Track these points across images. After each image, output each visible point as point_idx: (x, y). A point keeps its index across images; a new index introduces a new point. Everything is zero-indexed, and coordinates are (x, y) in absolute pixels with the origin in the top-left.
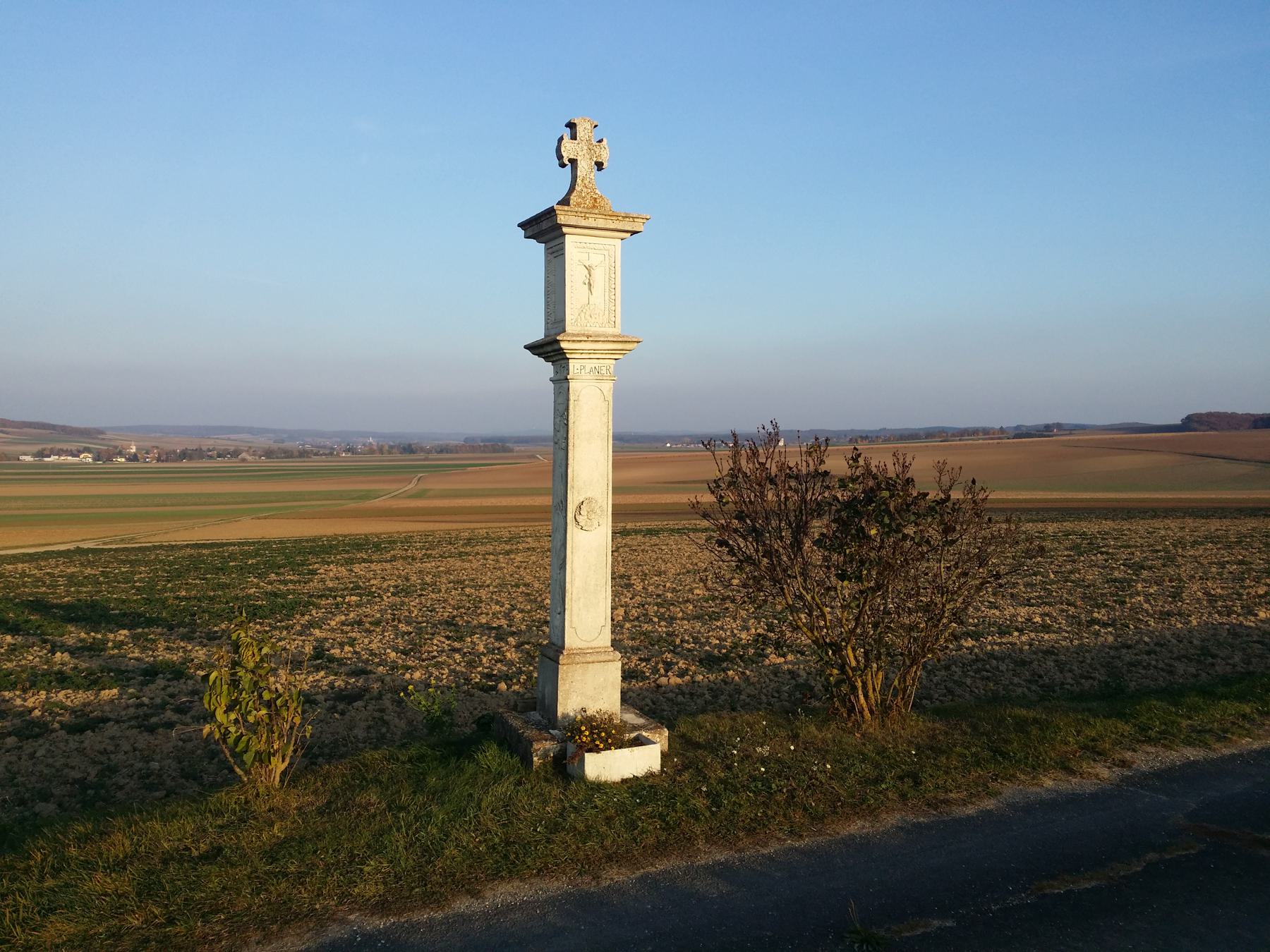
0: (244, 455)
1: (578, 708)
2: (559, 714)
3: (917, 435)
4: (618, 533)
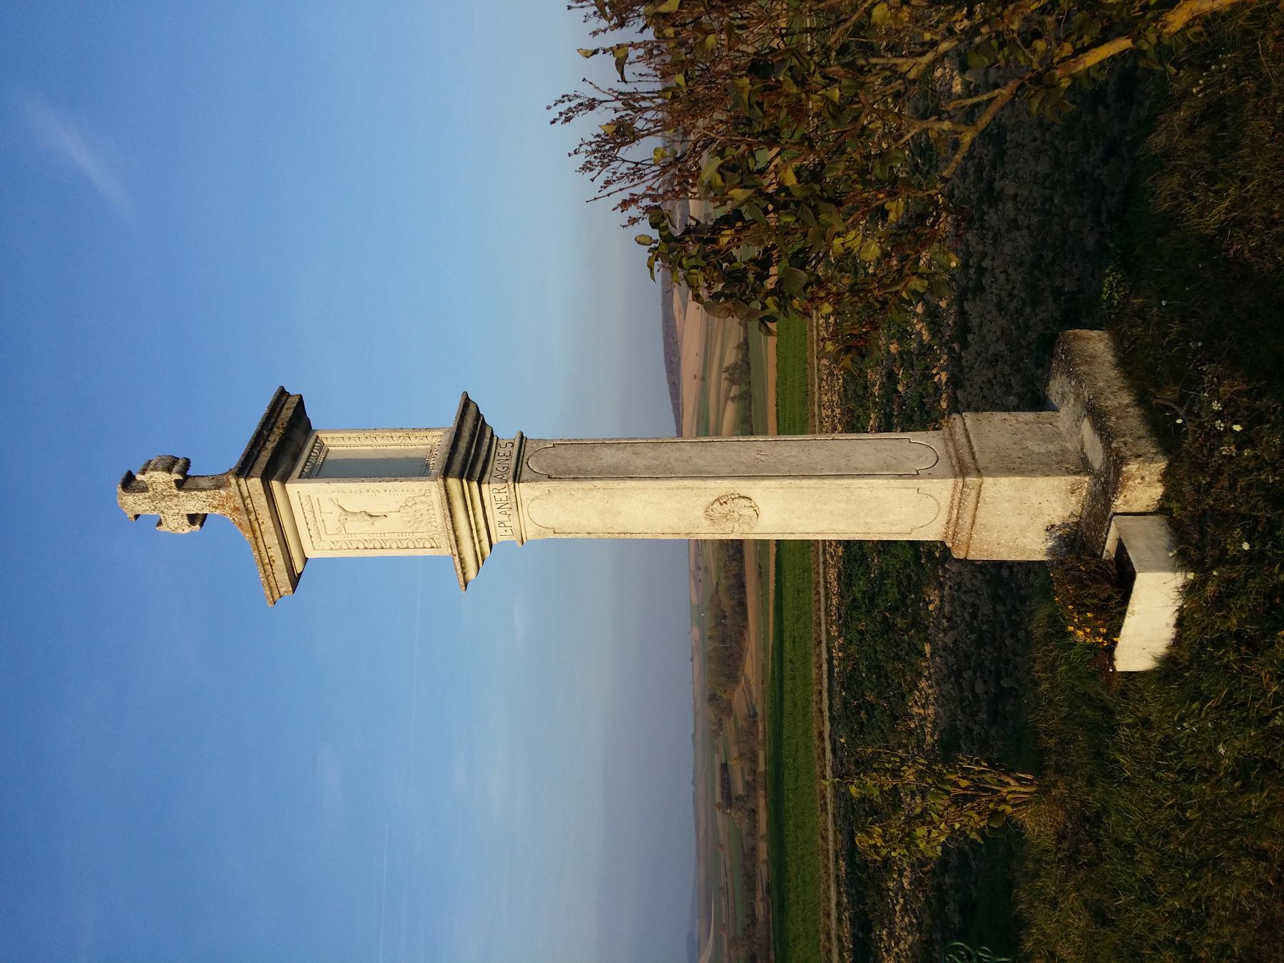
1: (1044, 535)
2: (1045, 558)
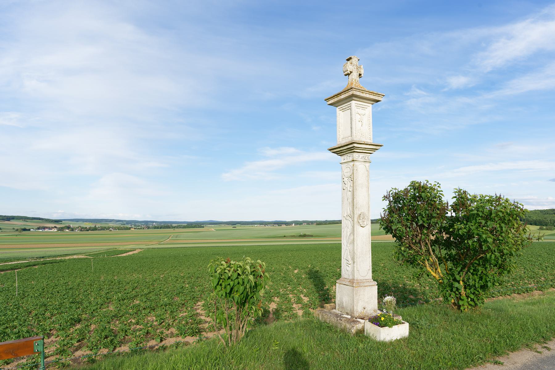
0: (111, 229)
3: (321, 223)
4: (341, 235)
